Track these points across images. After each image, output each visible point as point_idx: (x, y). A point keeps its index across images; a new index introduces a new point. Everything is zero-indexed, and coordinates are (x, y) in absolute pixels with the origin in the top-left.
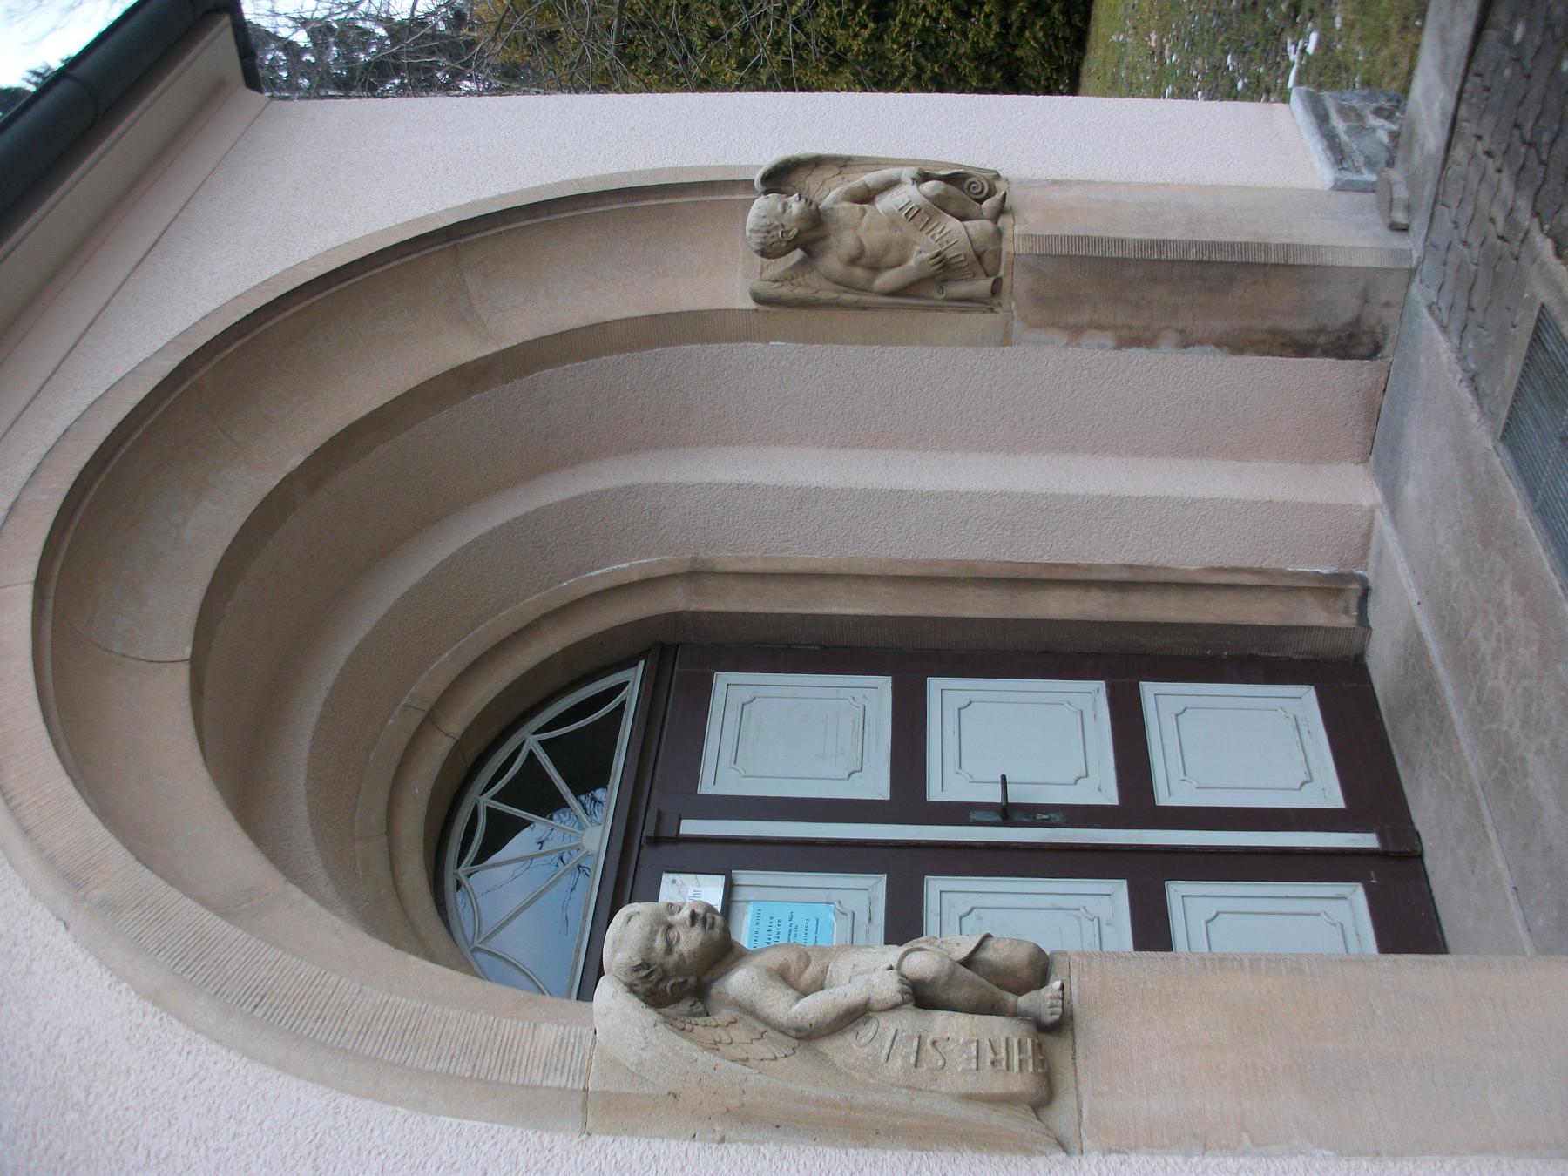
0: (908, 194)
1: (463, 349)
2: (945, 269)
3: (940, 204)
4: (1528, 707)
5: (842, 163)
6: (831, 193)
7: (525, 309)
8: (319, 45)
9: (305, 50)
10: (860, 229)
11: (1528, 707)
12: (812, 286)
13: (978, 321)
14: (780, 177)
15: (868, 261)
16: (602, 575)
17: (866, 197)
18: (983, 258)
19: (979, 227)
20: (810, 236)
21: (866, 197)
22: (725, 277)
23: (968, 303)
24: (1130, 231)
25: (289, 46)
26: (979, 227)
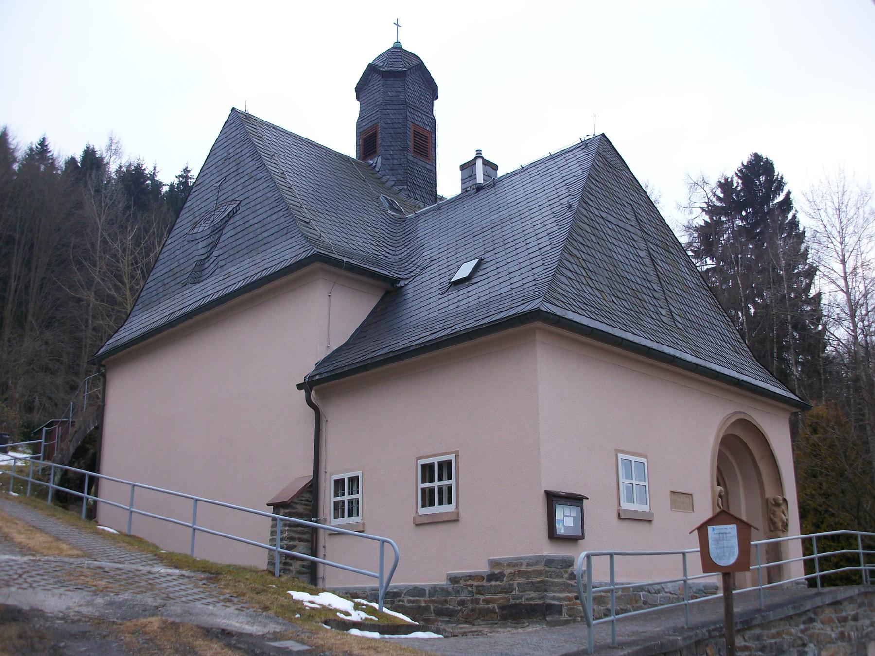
0: (784, 517)
1: (757, 458)
2: (774, 523)
3: (783, 522)
4: (451, 614)
5: (787, 509)
6: (783, 507)
7: (763, 466)
8: (808, 301)
9: (807, 296)
10: (779, 513)
11: (451, 614)
12: (770, 506)
13: (767, 529)
14: (785, 500)
15: (774, 513)
16: (726, 479)
17: (783, 512)
18: (776, 529)
19: (780, 528)
20: (777, 505)
21: (783, 512)
22: (770, 494)
23: (770, 527)
24: (782, 549)
25: (808, 287)
26: (780, 528)
